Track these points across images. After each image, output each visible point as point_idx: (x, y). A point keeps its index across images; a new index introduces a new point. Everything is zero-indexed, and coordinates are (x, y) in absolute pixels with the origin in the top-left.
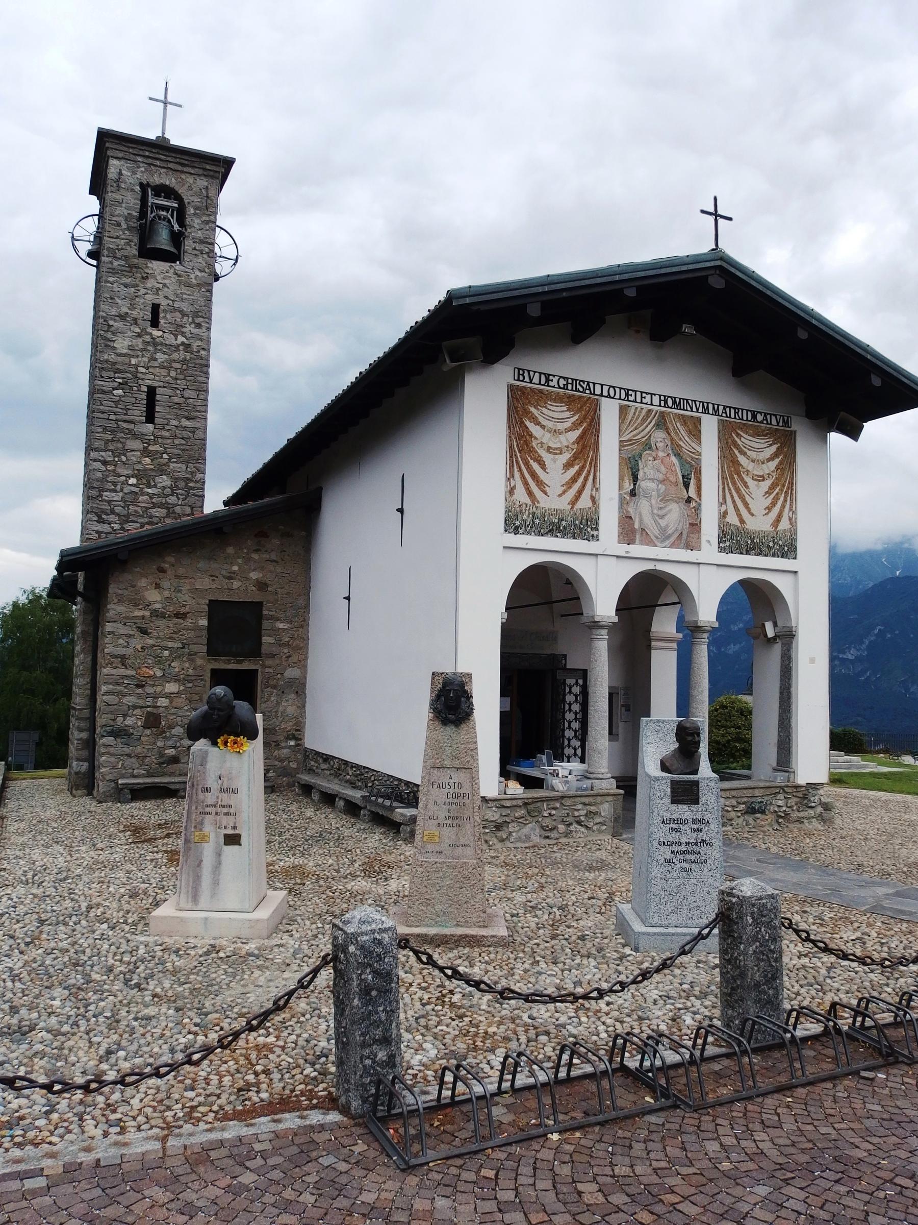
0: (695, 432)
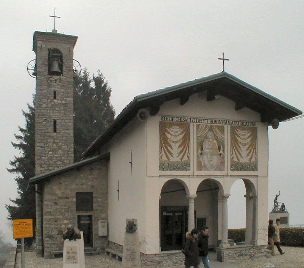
0: (222, 130)
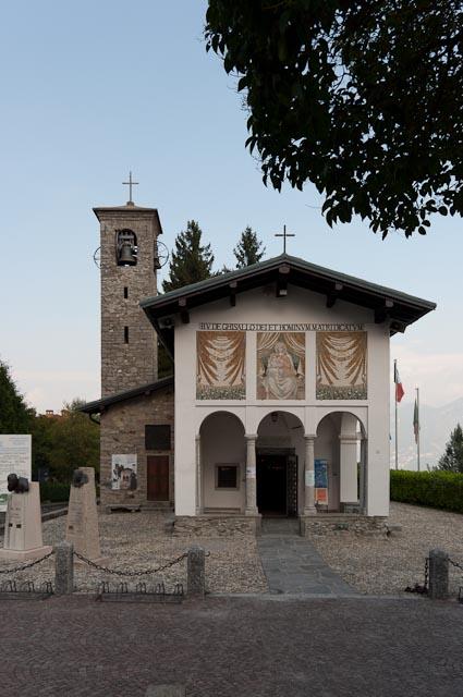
0: (301, 339)
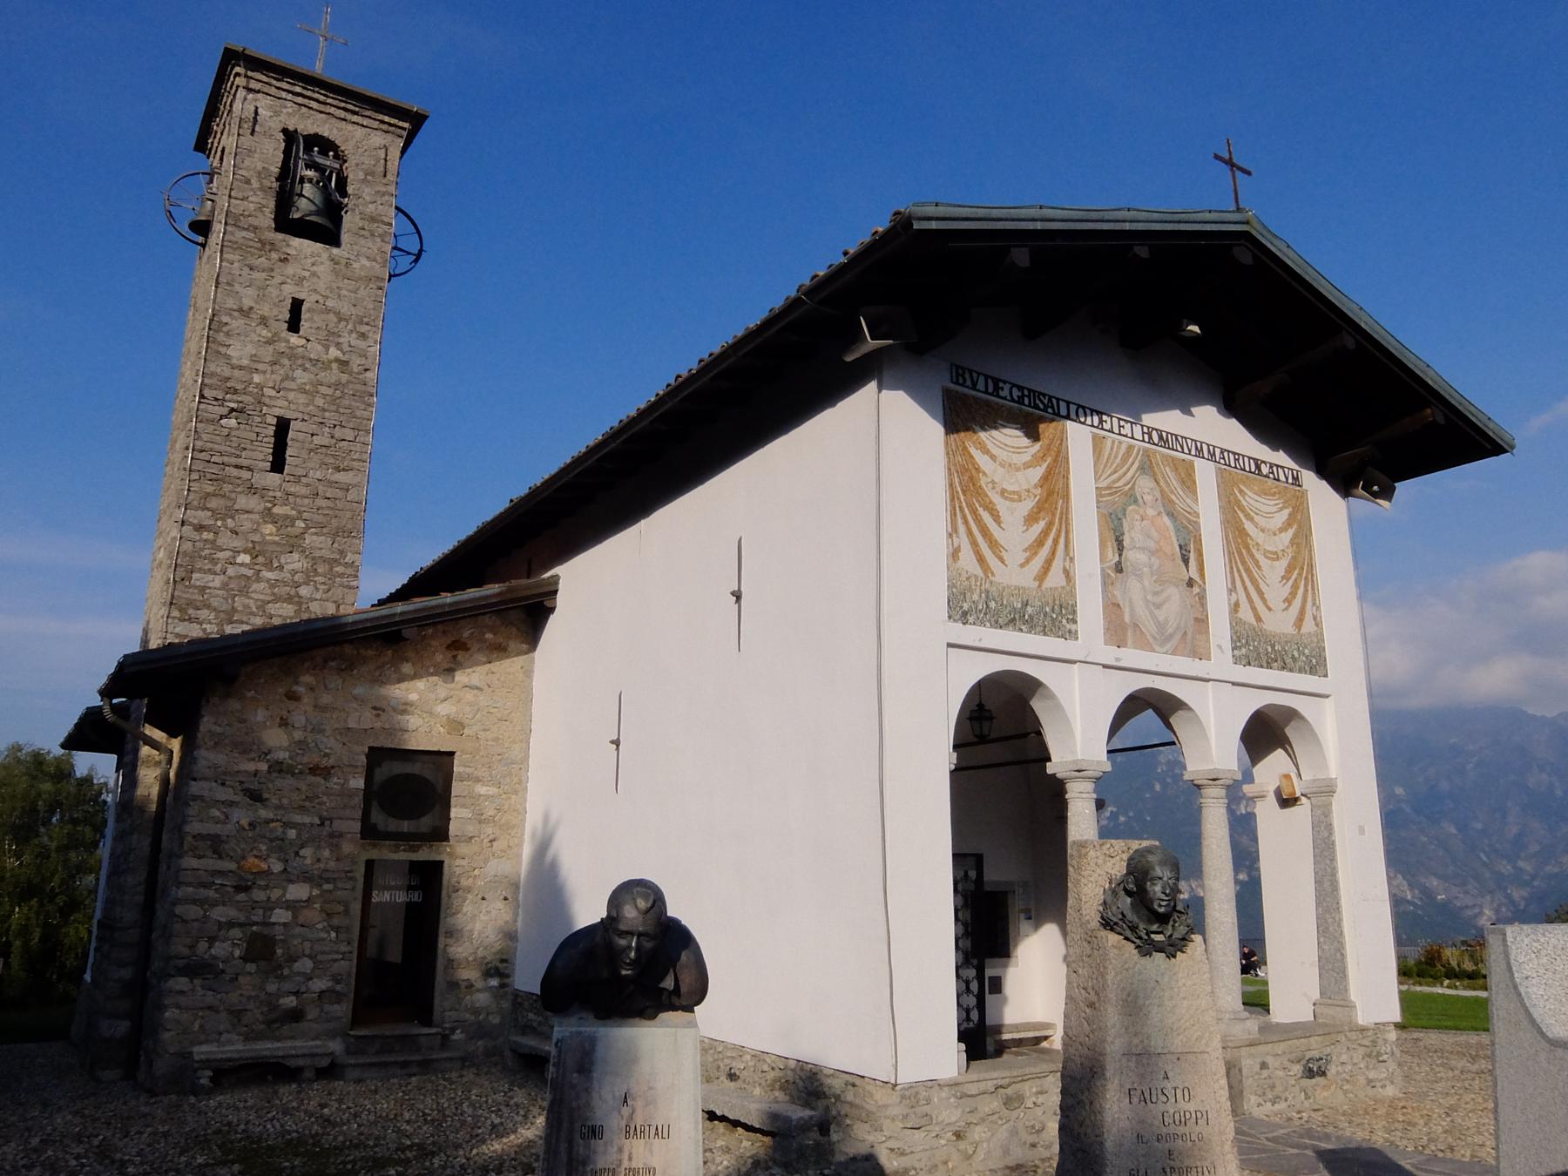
0: (1188, 482)
